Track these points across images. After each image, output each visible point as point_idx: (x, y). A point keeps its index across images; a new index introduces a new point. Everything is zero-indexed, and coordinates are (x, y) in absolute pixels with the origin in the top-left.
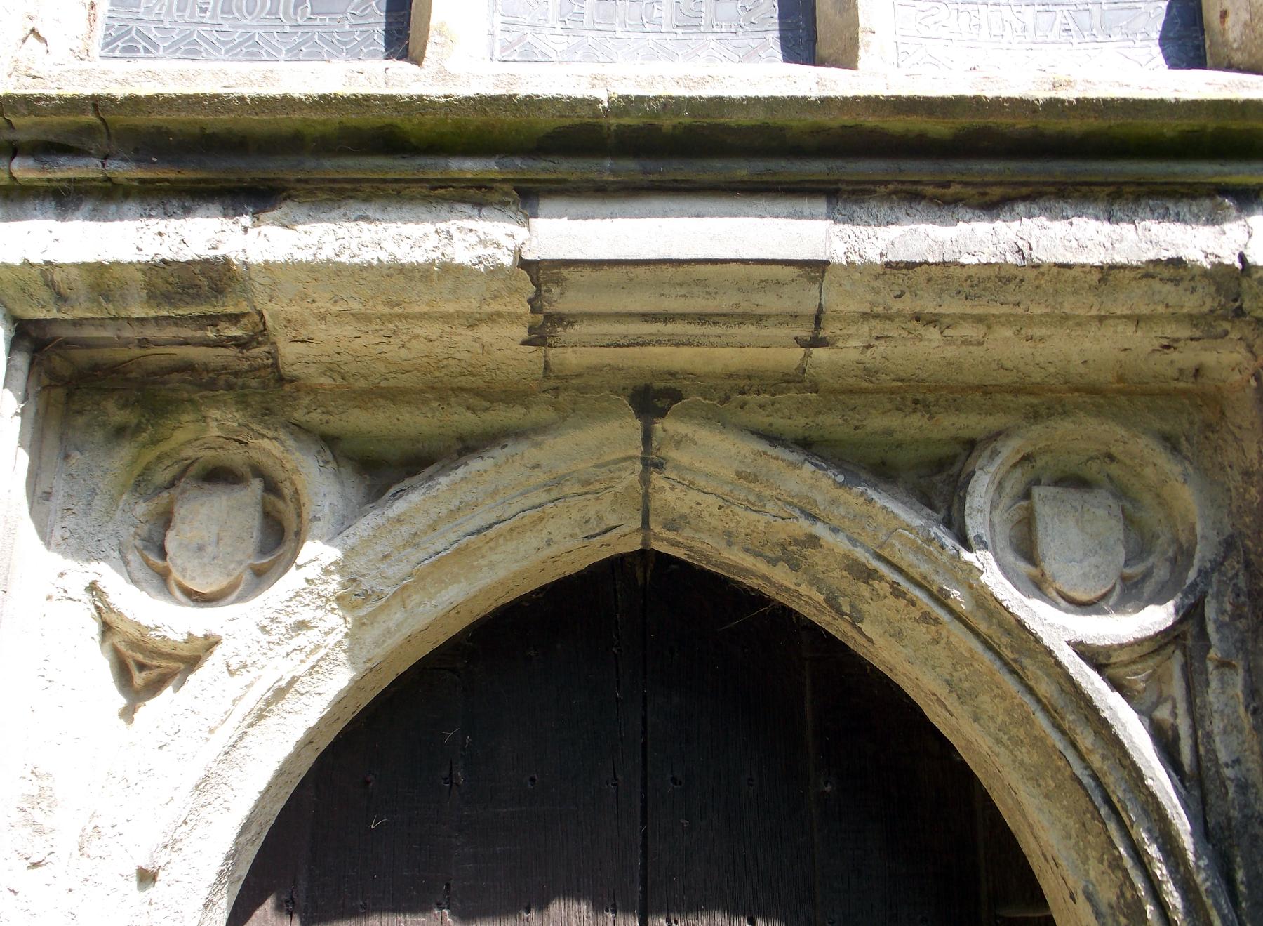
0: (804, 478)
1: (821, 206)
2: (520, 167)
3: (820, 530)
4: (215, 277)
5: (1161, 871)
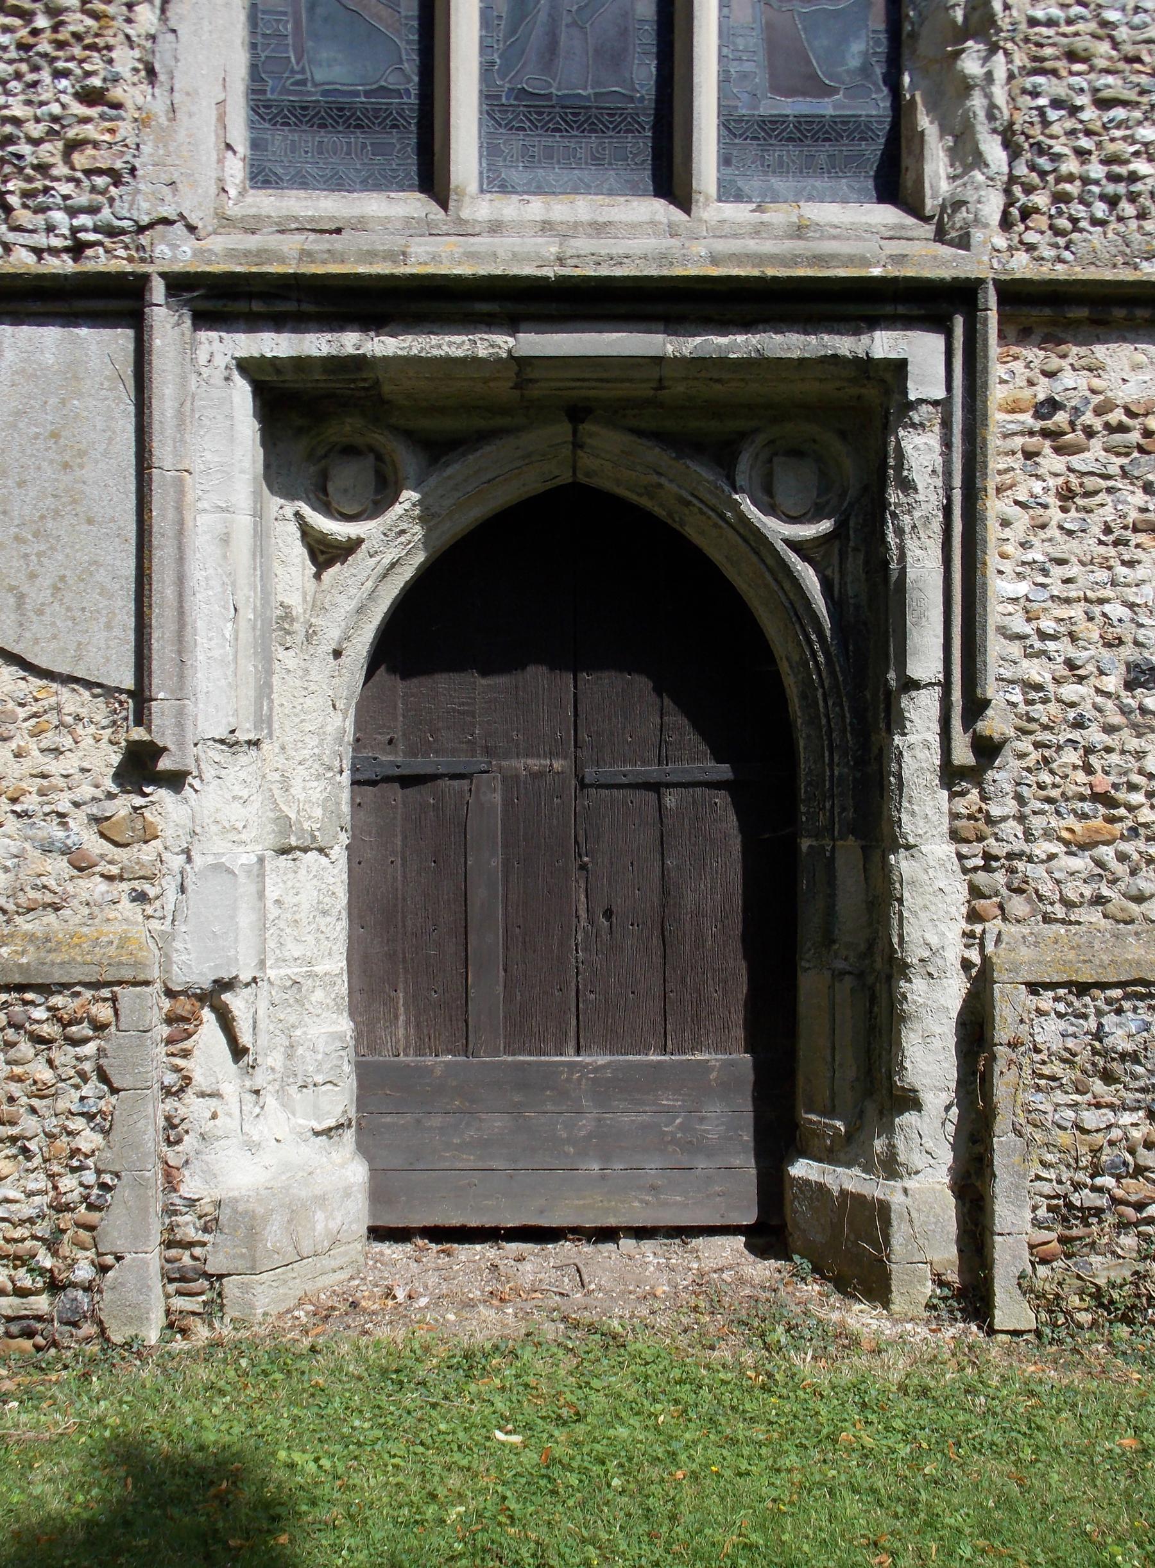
0: (655, 454)
2: (510, 307)
3: (663, 480)
4: (359, 362)
5: (817, 646)
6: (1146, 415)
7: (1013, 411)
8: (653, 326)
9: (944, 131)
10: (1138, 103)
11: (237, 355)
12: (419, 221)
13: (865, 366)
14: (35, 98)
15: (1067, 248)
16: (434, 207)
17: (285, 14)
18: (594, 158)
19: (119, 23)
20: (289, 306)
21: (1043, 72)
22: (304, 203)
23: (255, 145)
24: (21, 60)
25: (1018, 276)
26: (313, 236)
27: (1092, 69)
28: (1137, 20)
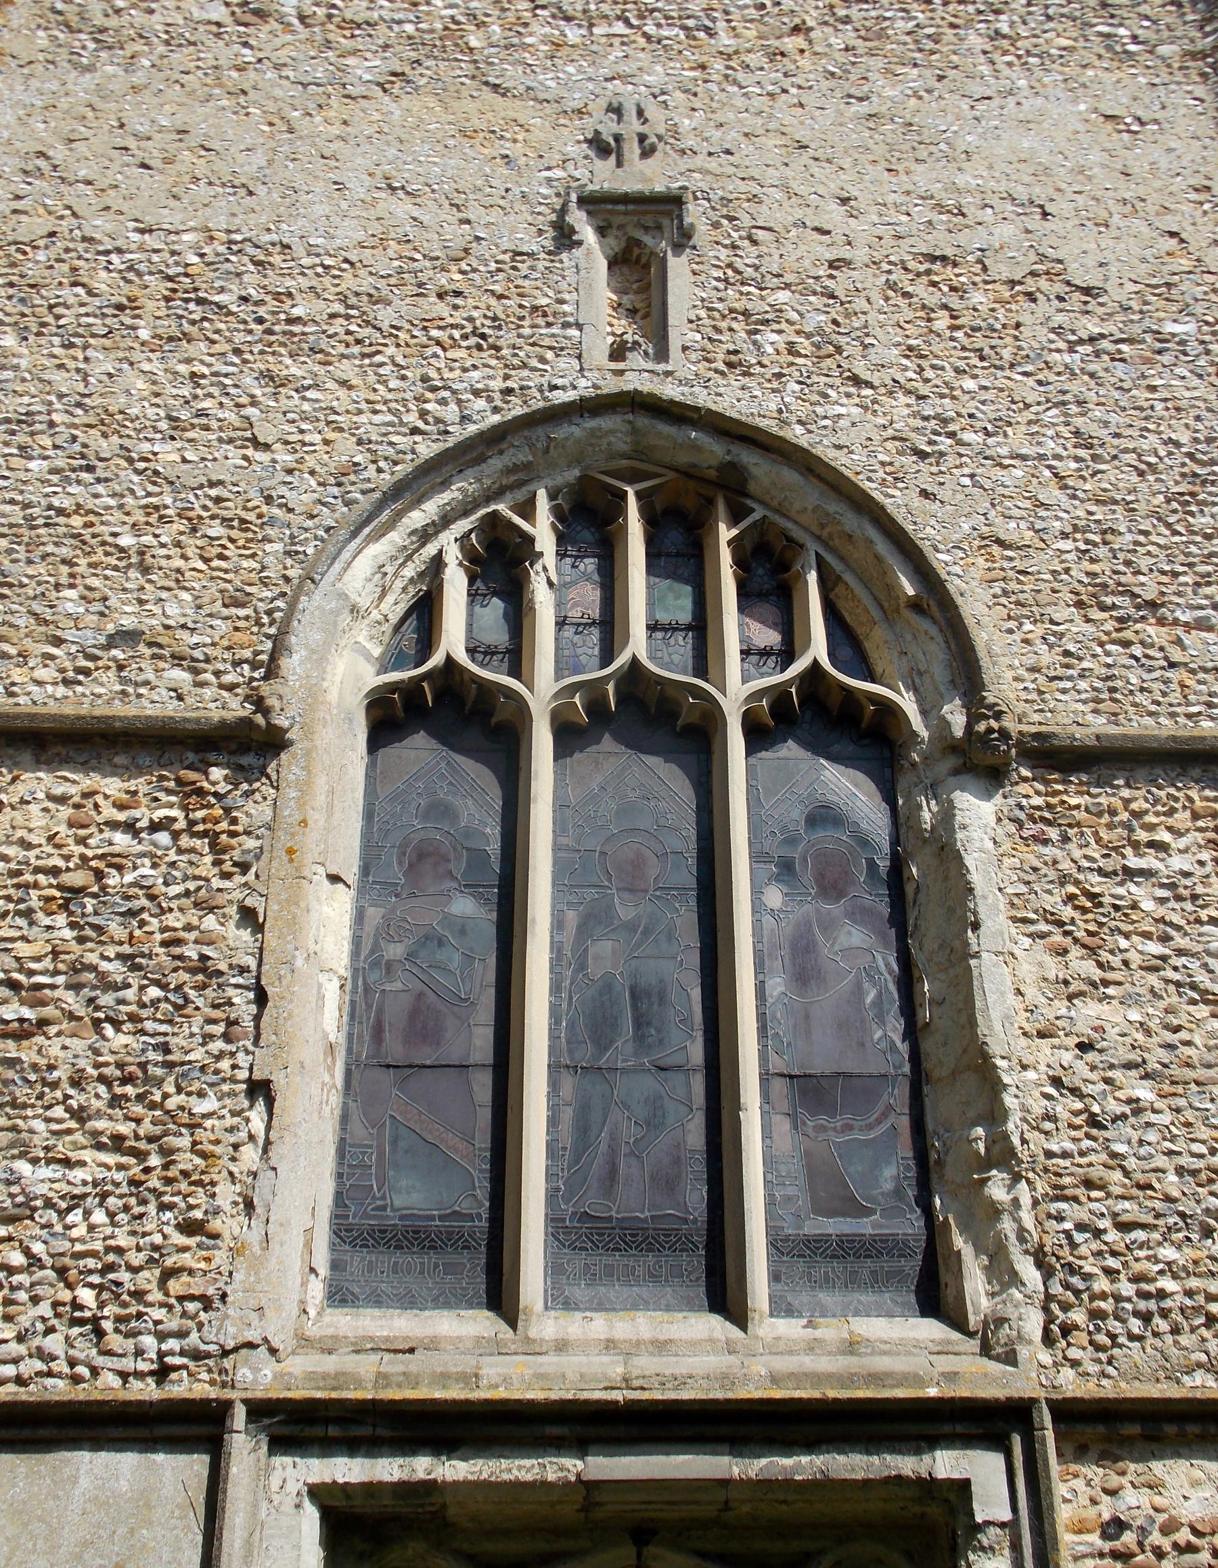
1: (726, 1448)
4: (429, 1487)
6: (1213, 1534)
7: (1080, 1532)
8: (719, 1448)
9: (978, 1250)
10: (1155, 1226)
11: (310, 1481)
12: (489, 1340)
13: (929, 1486)
14: (140, 1229)
15: (1110, 1363)
16: (503, 1326)
17: (370, 1147)
18: (652, 1275)
19: (225, 1161)
20: (366, 1431)
21: (1065, 1199)
22: (379, 1323)
23: (335, 1266)
24: (131, 1195)
25: (1069, 1395)
26: (387, 1357)
27: (1108, 1195)
28: (1142, 1151)
